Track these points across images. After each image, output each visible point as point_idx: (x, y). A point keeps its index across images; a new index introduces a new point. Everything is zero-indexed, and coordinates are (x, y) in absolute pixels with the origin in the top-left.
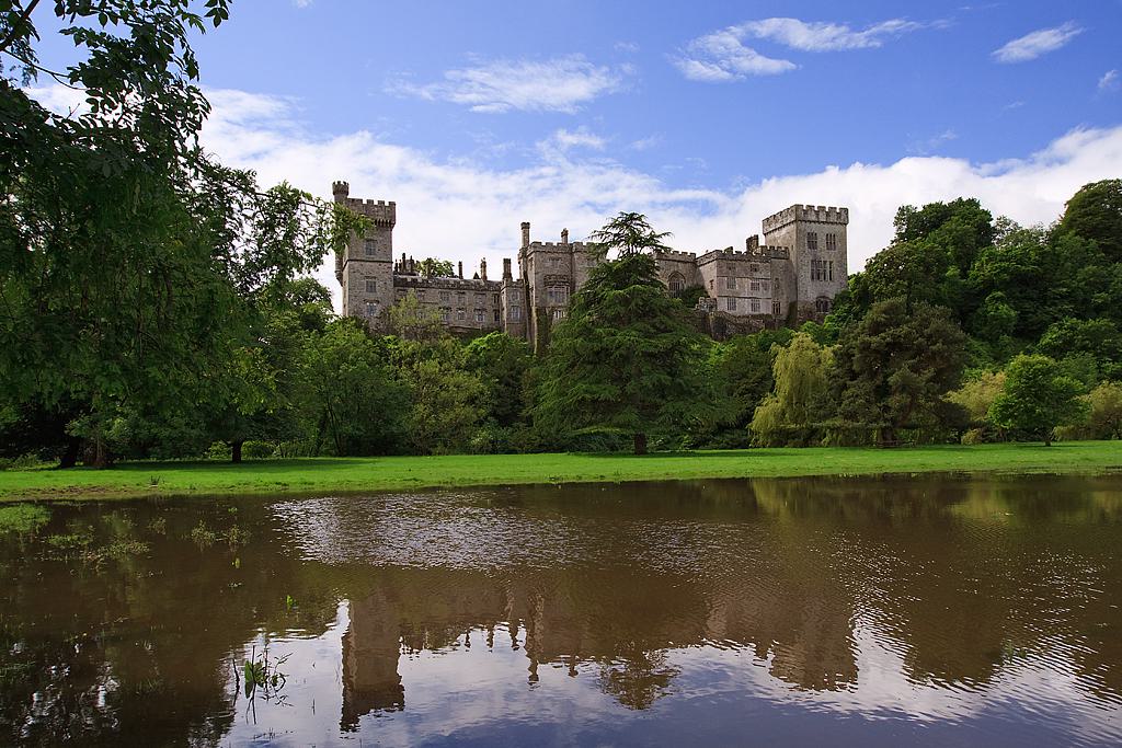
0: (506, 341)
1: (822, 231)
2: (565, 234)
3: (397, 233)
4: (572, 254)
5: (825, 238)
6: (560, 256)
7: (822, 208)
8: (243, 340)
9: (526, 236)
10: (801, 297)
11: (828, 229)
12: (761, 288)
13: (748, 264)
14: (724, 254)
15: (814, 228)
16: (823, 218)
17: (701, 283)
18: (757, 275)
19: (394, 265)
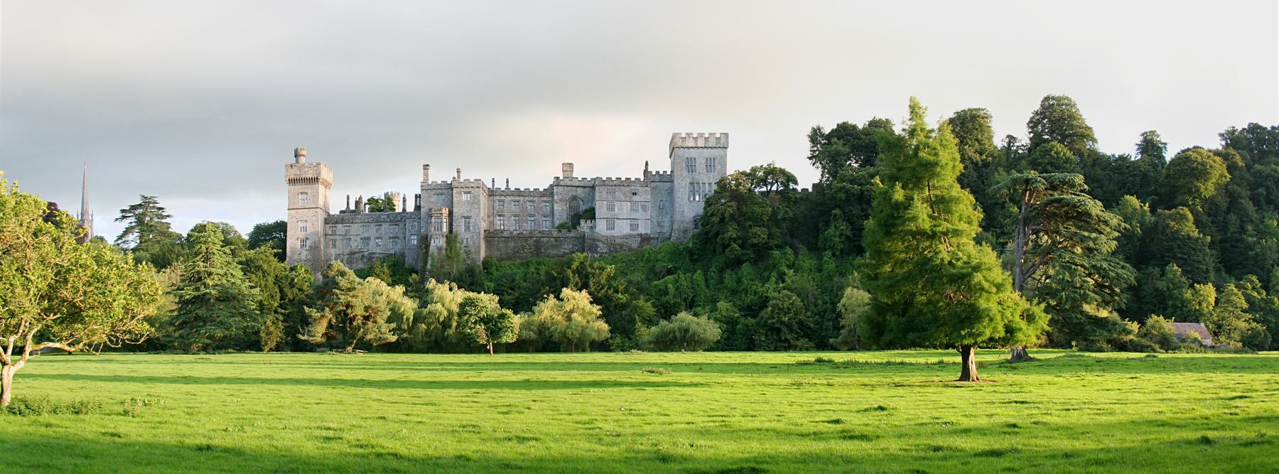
0: (472, 333)
1: (701, 157)
2: (569, 167)
3: (730, 152)
4: (452, 189)
5: (704, 161)
6: (444, 191)
7: (701, 135)
8: (80, 241)
9: (426, 175)
10: (678, 217)
11: (707, 153)
12: (640, 210)
13: (628, 189)
14: (604, 181)
15: (693, 153)
16: (701, 143)
17: (593, 205)
18: (636, 198)
19: (420, 336)
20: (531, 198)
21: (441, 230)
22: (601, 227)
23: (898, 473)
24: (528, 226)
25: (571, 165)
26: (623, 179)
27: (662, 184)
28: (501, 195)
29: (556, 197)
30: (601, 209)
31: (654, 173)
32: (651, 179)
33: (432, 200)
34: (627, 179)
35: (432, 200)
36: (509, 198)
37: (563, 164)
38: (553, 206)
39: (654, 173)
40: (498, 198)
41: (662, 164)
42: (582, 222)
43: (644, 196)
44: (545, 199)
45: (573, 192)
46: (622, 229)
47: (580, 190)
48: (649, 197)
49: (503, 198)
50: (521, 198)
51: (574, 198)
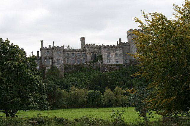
9: (42, 44)
12: (119, 56)
14: (106, 46)
20: (78, 52)
21: (49, 64)
22: (105, 62)
23: (188, 125)
24: (77, 63)
25: (84, 38)
26: (113, 45)
27: (126, 46)
28: (68, 51)
29: (87, 52)
30: (104, 56)
31: (123, 43)
32: (120, 44)
33: (45, 53)
34: (114, 45)
35: (45, 53)
36: (71, 52)
37: (84, 38)
38: (86, 55)
39: (123, 43)
40: (67, 52)
41: (125, 40)
42: (98, 60)
43: (120, 51)
44: (84, 52)
45: (93, 50)
46: (113, 62)
47: (96, 49)
48: (122, 51)
49: (68, 52)
50: (75, 52)
51: (94, 52)
